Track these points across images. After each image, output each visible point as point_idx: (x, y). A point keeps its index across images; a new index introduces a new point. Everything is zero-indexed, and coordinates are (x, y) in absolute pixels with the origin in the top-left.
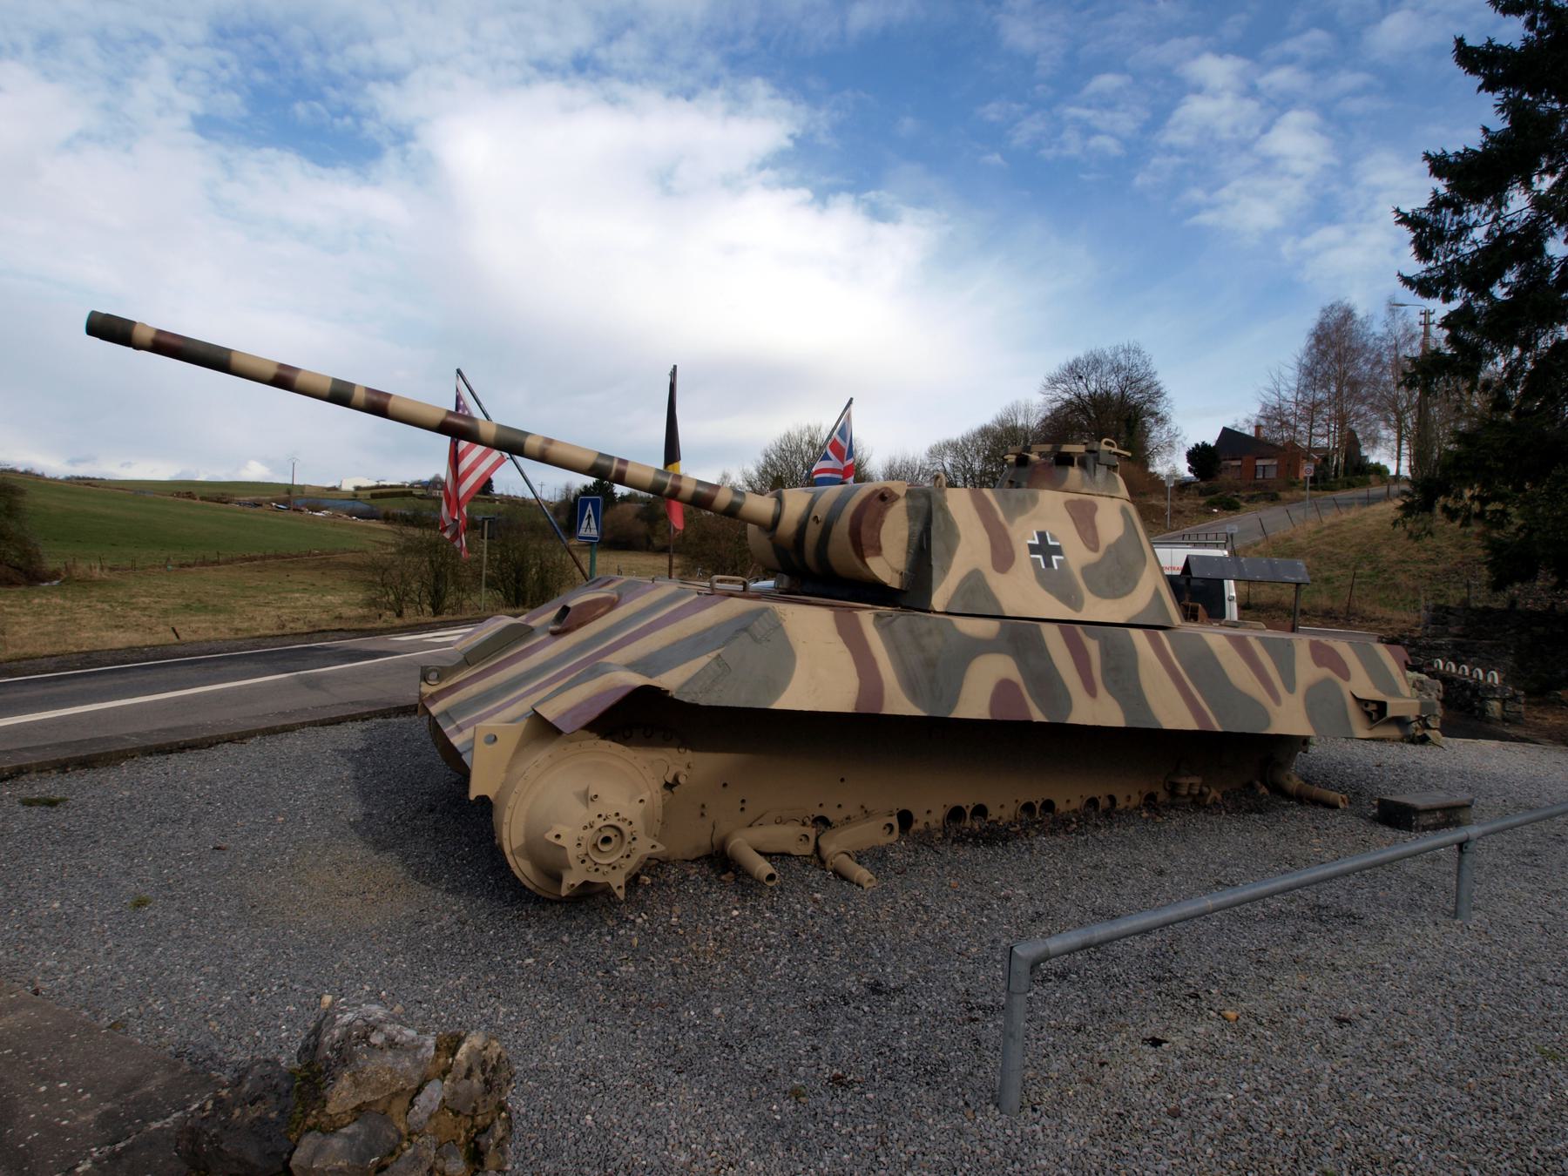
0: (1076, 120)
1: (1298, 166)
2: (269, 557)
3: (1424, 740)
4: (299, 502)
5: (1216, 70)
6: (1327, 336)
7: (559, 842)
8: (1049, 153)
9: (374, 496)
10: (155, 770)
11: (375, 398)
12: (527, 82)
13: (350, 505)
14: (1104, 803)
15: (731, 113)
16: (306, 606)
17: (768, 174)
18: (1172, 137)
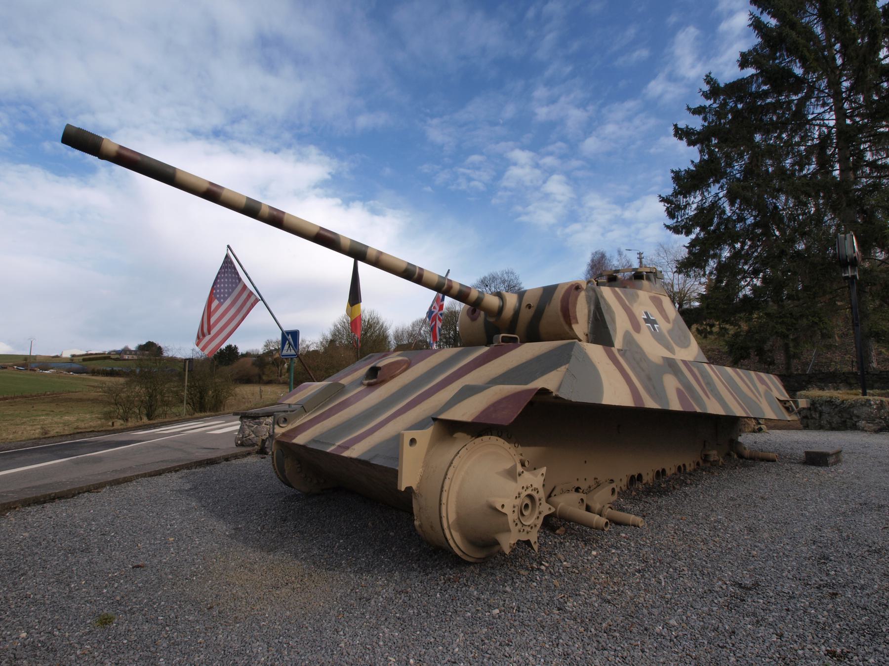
0: (464, 174)
1: (559, 198)
2: (17, 397)
3: (760, 430)
4: (33, 365)
5: (522, 156)
6: (595, 265)
7: (503, 511)
8: (453, 188)
9: (84, 360)
10: (34, 515)
11: (275, 213)
12: (186, 140)
13: (69, 366)
14: (648, 478)
15: (298, 160)
16: (51, 423)
17: (318, 191)
18: (505, 183)
